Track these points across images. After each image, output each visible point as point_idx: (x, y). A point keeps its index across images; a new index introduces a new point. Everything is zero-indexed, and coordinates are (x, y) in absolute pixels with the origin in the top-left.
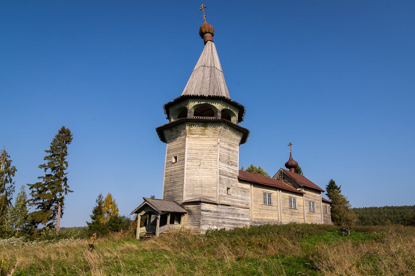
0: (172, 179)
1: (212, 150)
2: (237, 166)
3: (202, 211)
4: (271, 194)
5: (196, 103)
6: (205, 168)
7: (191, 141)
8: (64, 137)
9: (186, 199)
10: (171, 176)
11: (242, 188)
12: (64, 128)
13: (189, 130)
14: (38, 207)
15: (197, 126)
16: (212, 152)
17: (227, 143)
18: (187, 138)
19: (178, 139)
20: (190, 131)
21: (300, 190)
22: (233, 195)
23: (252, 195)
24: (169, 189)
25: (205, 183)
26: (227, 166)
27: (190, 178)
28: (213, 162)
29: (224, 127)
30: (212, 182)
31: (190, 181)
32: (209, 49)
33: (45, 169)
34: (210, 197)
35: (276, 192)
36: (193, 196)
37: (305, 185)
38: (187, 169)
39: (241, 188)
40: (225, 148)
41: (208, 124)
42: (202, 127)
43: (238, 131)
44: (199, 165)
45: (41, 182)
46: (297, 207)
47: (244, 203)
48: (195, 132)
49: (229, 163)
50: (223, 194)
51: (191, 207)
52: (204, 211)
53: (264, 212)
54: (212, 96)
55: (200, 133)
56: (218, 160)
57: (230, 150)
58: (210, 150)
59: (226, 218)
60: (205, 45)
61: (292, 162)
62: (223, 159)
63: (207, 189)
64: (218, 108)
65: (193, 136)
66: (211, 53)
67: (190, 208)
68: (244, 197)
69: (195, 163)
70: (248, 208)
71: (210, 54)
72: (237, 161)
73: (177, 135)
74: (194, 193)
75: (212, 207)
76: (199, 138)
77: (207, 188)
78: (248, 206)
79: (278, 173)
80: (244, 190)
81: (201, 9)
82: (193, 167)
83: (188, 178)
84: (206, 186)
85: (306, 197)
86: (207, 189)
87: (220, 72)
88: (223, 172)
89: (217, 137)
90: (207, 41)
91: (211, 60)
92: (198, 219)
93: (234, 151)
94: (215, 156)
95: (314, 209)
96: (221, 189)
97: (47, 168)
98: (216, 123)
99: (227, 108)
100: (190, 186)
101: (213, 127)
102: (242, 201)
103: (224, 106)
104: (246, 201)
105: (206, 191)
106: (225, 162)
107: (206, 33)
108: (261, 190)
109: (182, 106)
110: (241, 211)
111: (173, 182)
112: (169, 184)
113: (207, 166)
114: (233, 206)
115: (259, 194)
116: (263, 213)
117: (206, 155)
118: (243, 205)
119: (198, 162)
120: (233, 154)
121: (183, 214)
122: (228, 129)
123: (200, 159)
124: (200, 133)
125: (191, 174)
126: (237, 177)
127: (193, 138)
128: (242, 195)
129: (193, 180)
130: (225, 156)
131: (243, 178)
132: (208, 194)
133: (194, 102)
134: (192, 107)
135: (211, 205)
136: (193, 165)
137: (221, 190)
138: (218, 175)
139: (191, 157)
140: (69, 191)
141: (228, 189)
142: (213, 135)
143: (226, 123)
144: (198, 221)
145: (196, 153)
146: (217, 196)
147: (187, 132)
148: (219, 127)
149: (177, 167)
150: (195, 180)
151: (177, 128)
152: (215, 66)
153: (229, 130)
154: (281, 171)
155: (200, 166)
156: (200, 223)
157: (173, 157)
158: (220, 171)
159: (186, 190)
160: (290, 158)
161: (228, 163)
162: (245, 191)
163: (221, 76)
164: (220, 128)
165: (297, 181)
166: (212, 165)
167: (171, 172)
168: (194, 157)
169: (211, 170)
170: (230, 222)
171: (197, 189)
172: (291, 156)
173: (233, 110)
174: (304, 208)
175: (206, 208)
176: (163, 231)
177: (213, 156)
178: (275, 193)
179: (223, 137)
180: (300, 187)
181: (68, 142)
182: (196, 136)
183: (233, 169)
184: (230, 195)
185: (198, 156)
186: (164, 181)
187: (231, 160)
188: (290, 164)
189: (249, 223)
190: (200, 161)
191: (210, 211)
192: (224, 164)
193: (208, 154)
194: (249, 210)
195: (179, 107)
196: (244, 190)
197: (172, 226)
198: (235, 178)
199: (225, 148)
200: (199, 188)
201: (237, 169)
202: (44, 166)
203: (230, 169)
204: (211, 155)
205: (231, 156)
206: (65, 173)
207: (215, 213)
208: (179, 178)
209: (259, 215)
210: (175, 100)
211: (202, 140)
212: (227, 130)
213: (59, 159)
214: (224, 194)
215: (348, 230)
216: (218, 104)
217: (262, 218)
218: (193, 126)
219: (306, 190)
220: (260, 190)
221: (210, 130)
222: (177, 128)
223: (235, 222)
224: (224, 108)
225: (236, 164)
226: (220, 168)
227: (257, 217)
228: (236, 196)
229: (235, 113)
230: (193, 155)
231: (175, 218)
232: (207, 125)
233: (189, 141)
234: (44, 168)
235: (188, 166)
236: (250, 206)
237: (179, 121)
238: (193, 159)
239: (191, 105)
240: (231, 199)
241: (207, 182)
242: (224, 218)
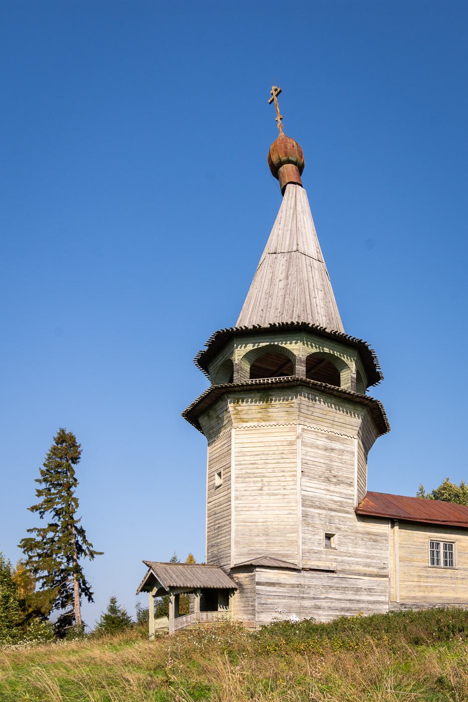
0: (217, 522)
2: (353, 486)
3: (258, 584)
4: (454, 543)
5: (250, 347)
6: (274, 495)
8: (66, 451)
10: (214, 516)
11: (369, 533)
12: (64, 433)
13: (235, 412)
14: (43, 585)
15: (250, 400)
16: (286, 457)
17: (323, 434)
18: (233, 431)
19: (221, 434)
20: (237, 414)
22: (342, 549)
24: (214, 542)
25: (274, 527)
26: (323, 487)
27: (243, 517)
28: (288, 479)
29: (309, 398)
30: (287, 523)
31: (243, 524)
33: (40, 513)
34: (284, 556)
36: (250, 554)
38: (237, 498)
39: (363, 534)
40: (317, 447)
43: (348, 403)
44: (260, 488)
45: (33, 537)
47: (373, 565)
48: (249, 414)
49: (330, 478)
50: (315, 548)
51: (242, 576)
53: (431, 582)
54: (310, 325)
55: (259, 415)
56: (299, 474)
57: (333, 450)
58: (282, 453)
59: (323, 597)
60: (283, 196)
62: (314, 472)
64: (295, 353)
65: (245, 425)
66: (293, 214)
68: (373, 552)
69: (252, 485)
70: (386, 576)
71: (295, 218)
72: (353, 472)
74: (253, 548)
75: (284, 576)
76: (258, 428)
77: (278, 536)
78: (385, 570)
80: (374, 537)
81: (271, 99)
82: (247, 493)
83: (239, 517)
86: (278, 538)
87: (316, 263)
88: (314, 499)
89: (295, 422)
90: (286, 186)
91: (291, 234)
92: (252, 602)
93: (343, 451)
96: (309, 537)
97: (44, 512)
98: (292, 388)
99: (323, 350)
100: (243, 534)
101: (283, 400)
102: (368, 560)
103: (312, 346)
104: (379, 561)
105: (276, 543)
107: (281, 164)
108: (423, 537)
109: (225, 357)
110: (365, 582)
111: (219, 527)
112: (213, 533)
113: (276, 490)
114: (343, 571)
115: (419, 544)
116: (429, 584)
117: (274, 465)
118: (371, 569)
119: (257, 482)
120: (340, 459)
121: (232, 590)
122: (320, 401)
123: (262, 474)
124: (259, 415)
125: (244, 509)
126: (352, 511)
128: (367, 548)
130: (318, 464)
131: (373, 508)
132: (281, 548)
133: (244, 345)
134: (241, 357)
135: (281, 572)
136: (248, 488)
137: (310, 539)
139: (244, 471)
141: (328, 537)
142: (286, 418)
143: (309, 387)
145: (253, 462)
147: (233, 417)
148: (296, 397)
150: (253, 520)
151: (216, 411)
153: (324, 402)
155: (261, 490)
156: (254, 610)
157: (216, 474)
158: (304, 499)
161: (328, 480)
162: (375, 539)
163: (317, 272)
164: (301, 400)
166: (287, 487)
167: (215, 507)
168: (249, 471)
169: (285, 497)
170: (333, 605)
171: (257, 539)
175: (269, 578)
176: (185, 625)
179: (310, 421)
181: (75, 460)
182: (252, 424)
183: (341, 493)
185: (257, 468)
187: (334, 473)
189: (387, 607)
190: (262, 480)
191: (280, 583)
192: (316, 482)
193: (278, 463)
195: (221, 362)
196: (374, 537)
197: (207, 614)
198: (347, 512)
199: (317, 447)
200: (262, 538)
203: (333, 492)
204: (284, 465)
205: (335, 464)
207: (293, 587)
208: (225, 519)
209: (416, 589)
210: (370, 353)
211: (264, 431)
213: (63, 494)
214: (319, 549)
216: (296, 343)
217: (426, 595)
218: (243, 401)
221: (278, 407)
223: (348, 605)
224: (314, 350)
225: (348, 481)
226: (303, 493)
227: (413, 594)
228: (351, 550)
230: (246, 467)
232: (270, 397)
233: (238, 436)
234: (38, 511)
235: (237, 492)
236: (390, 571)
238: (248, 475)
239: (240, 353)
240: (336, 557)
242: (318, 599)
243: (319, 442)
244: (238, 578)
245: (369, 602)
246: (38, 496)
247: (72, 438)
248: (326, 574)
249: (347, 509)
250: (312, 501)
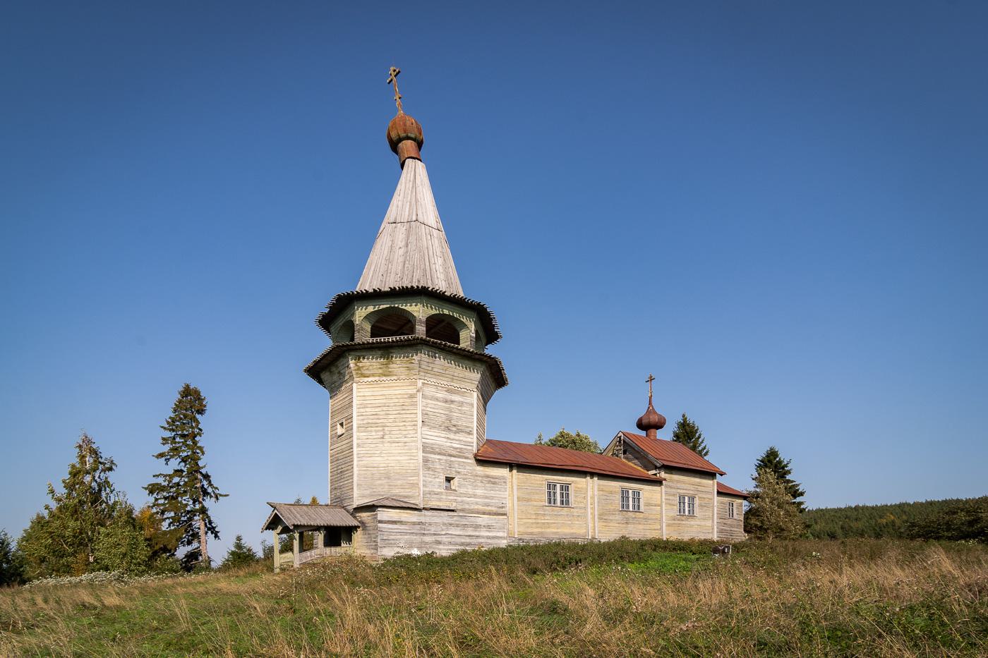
0: (340, 467)
1: (407, 404)
2: (472, 434)
3: (380, 522)
4: (570, 484)
5: (371, 309)
7: (363, 390)
9: (358, 501)
11: (488, 477)
13: (356, 368)
16: (407, 408)
17: (443, 387)
18: (355, 385)
20: (358, 369)
21: (655, 474)
22: (462, 490)
23: (515, 488)
26: (443, 435)
29: (429, 355)
30: (408, 468)
32: (408, 178)
33: (166, 460)
34: (406, 497)
35: (584, 480)
36: (372, 495)
37: (666, 463)
40: (437, 399)
41: (392, 351)
42: (382, 360)
43: (468, 360)
46: (642, 508)
49: (450, 427)
51: (364, 516)
52: (385, 523)
54: (430, 289)
55: (380, 371)
56: (420, 423)
57: (452, 402)
58: (403, 405)
59: (443, 533)
61: (651, 417)
63: (399, 482)
65: (366, 379)
67: (363, 519)
69: (374, 434)
70: (505, 514)
71: (414, 191)
73: (341, 381)
77: (399, 479)
79: (614, 442)
80: (492, 480)
81: (390, 79)
82: (369, 441)
84: (397, 477)
85: (666, 486)
87: (435, 233)
89: (415, 377)
90: (404, 161)
91: (410, 206)
94: (412, 416)
95: (692, 511)
96: (430, 479)
97: (169, 459)
103: (432, 308)
106: (437, 426)
107: (400, 140)
110: (483, 520)
114: (463, 510)
118: (490, 508)
119: (378, 431)
121: (356, 528)
122: (440, 358)
124: (380, 371)
125: (367, 455)
126: (471, 456)
127: (368, 383)
129: (372, 465)
130: (438, 415)
131: (492, 454)
135: (402, 511)
138: (421, 454)
139: (365, 422)
140: (221, 495)
141: (449, 480)
144: (374, 541)
146: (420, 494)
148: (417, 355)
149: (342, 444)
150: (375, 465)
152: (421, 219)
153: (444, 359)
154: (620, 437)
155: (383, 438)
159: (358, 485)
160: (649, 408)
161: (448, 429)
162: (493, 481)
163: (436, 241)
165: (650, 456)
168: (370, 421)
171: (379, 482)
172: (650, 403)
173: (460, 314)
174: (662, 508)
175: (391, 517)
177: (408, 416)
178: (577, 482)
179: (429, 375)
180: (656, 468)
184: (455, 490)
186: (329, 471)
187: (454, 422)
188: (645, 421)
190: (384, 430)
191: (402, 522)
194: (505, 517)
196: (492, 480)
199: (437, 399)
201: (473, 439)
202: (161, 455)
203: (453, 440)
204: (405, 416)
206: (201, 465)
208: (347, 465)
209: (534, 526)
211: (386, 385)
212: (438, 359)
214: (439, 490)
215: (729, 550)
216: (416, 305)
217: (543, 530)
218: (364, 358)
219: (672, 474)
220: (538, 478)
221: (398, 363)
222: (337, 366)
224: (434, 312)
225: (468, 430)
227: (530, 530)
229: (464, 320)
231: (342, 537)
234: (164, 458)
236: (506, 510)
237: (333, 352)
239: (361, 314)
240: (455, 498)
241: (400, 469)
243: (439, 395)
244: (360, 517)
245: (488, 538)
248: (446, 513)
250: (432, 448)
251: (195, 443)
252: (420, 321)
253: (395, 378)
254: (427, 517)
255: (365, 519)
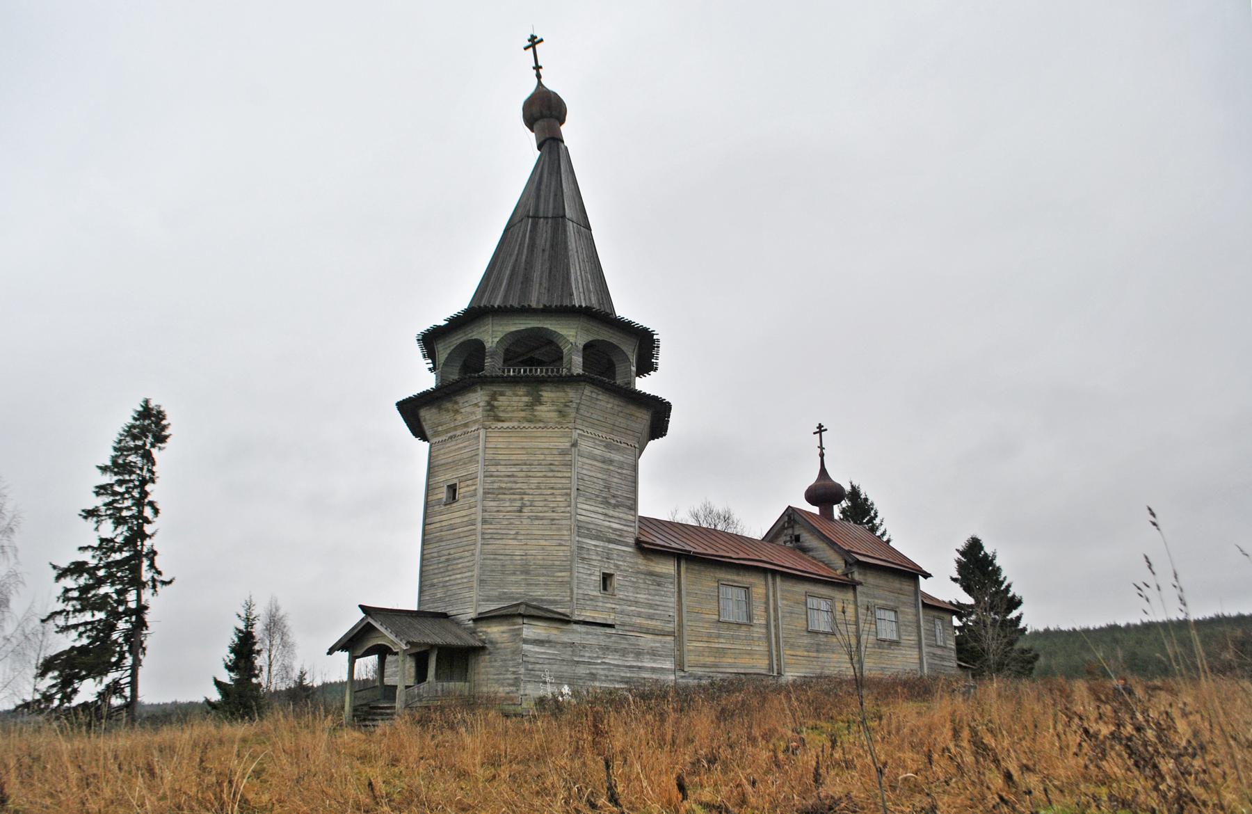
3: (526, 641)
6: (537, 518)
11: (651, 574)
26: (600, 510)
51: (495, 631)
56: (574, 493)
57: (611, 462)
65: (500, 425)
94: (564, 481)
111: (448, 560)
139: (496, 486)
150: (508, 552)
161: (606, 502)
168: (504, 485)
171: (513, 578)
204: (553, 480)
243: (597, 452)
244: (486, 633)
245: (653, 670)
246: (98, 494)
247: (160, 416)
248: (600, 630)
249: (627, 540)
250: (588, 529)
251: (144, 494)
252: (574, 345)
253: (541, 425)
254: (577, 634)
255: (497, 636)
